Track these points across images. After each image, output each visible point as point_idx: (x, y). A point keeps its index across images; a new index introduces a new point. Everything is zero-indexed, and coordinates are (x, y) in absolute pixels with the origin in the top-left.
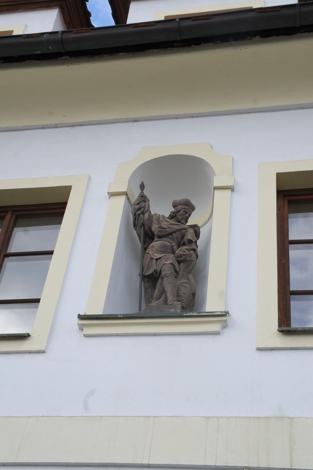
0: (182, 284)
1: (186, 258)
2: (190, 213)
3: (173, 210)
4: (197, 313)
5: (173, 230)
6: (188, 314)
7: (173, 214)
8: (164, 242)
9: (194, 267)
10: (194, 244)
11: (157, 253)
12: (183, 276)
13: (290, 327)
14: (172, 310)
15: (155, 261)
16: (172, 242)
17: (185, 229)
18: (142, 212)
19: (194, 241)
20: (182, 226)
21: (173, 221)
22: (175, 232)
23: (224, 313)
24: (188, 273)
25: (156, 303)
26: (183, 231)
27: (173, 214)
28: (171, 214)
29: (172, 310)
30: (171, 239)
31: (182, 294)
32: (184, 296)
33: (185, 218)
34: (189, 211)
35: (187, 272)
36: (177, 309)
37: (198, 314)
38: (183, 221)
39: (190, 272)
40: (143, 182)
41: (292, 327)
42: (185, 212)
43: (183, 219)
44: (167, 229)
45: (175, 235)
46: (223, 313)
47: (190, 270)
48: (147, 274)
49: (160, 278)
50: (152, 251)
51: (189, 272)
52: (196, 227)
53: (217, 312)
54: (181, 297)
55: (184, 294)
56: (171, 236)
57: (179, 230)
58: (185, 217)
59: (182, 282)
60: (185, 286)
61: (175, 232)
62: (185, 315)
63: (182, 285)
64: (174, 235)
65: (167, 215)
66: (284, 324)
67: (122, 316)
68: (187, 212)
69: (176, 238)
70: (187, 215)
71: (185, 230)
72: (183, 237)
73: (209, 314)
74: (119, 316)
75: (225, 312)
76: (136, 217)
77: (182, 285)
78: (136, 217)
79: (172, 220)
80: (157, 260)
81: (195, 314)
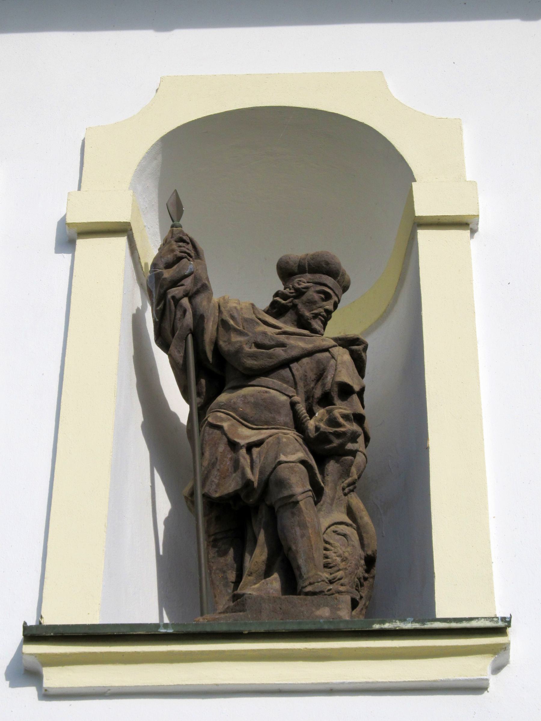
0: (333, 528)
1: (342, 445)
2: (336, 299)
3: (280, 286)
4: (415, 621)
5: (294, 353)
6: (387, 626)
7: (283, 302)
8: (266, 392)
9: (362, 472)
10: (355, 397)
11: (243, 424)
12: (333, 500)
13: (179, 222)
14: (325, 612)
15: (243, 451)
16: (291, 391)
17: (327, 350)
18: (185, 291)
19: (357, 388)
20: (318, 342)
21: (285, 322)
22: (297, 359)
23: (501, 624)
24: (347, 490)
25: (258, 589)
26: (319, 355)
27: (283, 302)
28: (278, 299)
29: (325, 612)
30: (287, 382)
31: (339, 559)
32: (342, 565)
33: (324, 314)
34: (334, 292)
35: (343, 489)
36: (339, 609)
37: (417, 626)
38: (316, 324)
39: (352, 491)
40: (176, 191)
41: (180, 222)
42: (323, 296)
43: (316, 316)
44: (271, 351)
45: (297, 370)
46: (497, 622)
47: (353, 483)
48: (217, 495)
49: (263, 512)
50: (229, 420)
51: (351, 488)
52: (358, 345)
53: (477, 618)
54: (336, 569)
55: (343, 560)
56: (286, 372)
57: (310, 354)
58: (321, 310)
59: (333, 522)
60: (345, 535)
61: (297, 359)
62: (376, 626)
63: (335, 532)
64: (295, 366)
65: (264, 303)
66: (332, 470)
67: (170, 631)
68: (328, 296)
69: (301, 379)
70: (329, 305)
71: (327, 354)
72: (320, 376)
73: (454, 625)
74: (163, 630)
75: (503, 619)
76: (165, 305)
77: (335, 532)
78: (165, 305)
79: (283, 319)
80: (249, 448)
81: (408, 626)
